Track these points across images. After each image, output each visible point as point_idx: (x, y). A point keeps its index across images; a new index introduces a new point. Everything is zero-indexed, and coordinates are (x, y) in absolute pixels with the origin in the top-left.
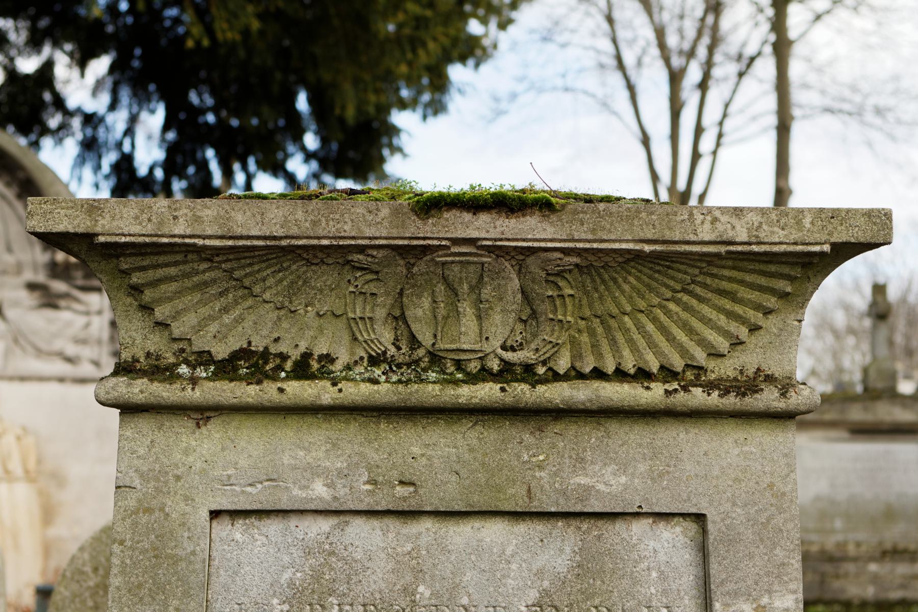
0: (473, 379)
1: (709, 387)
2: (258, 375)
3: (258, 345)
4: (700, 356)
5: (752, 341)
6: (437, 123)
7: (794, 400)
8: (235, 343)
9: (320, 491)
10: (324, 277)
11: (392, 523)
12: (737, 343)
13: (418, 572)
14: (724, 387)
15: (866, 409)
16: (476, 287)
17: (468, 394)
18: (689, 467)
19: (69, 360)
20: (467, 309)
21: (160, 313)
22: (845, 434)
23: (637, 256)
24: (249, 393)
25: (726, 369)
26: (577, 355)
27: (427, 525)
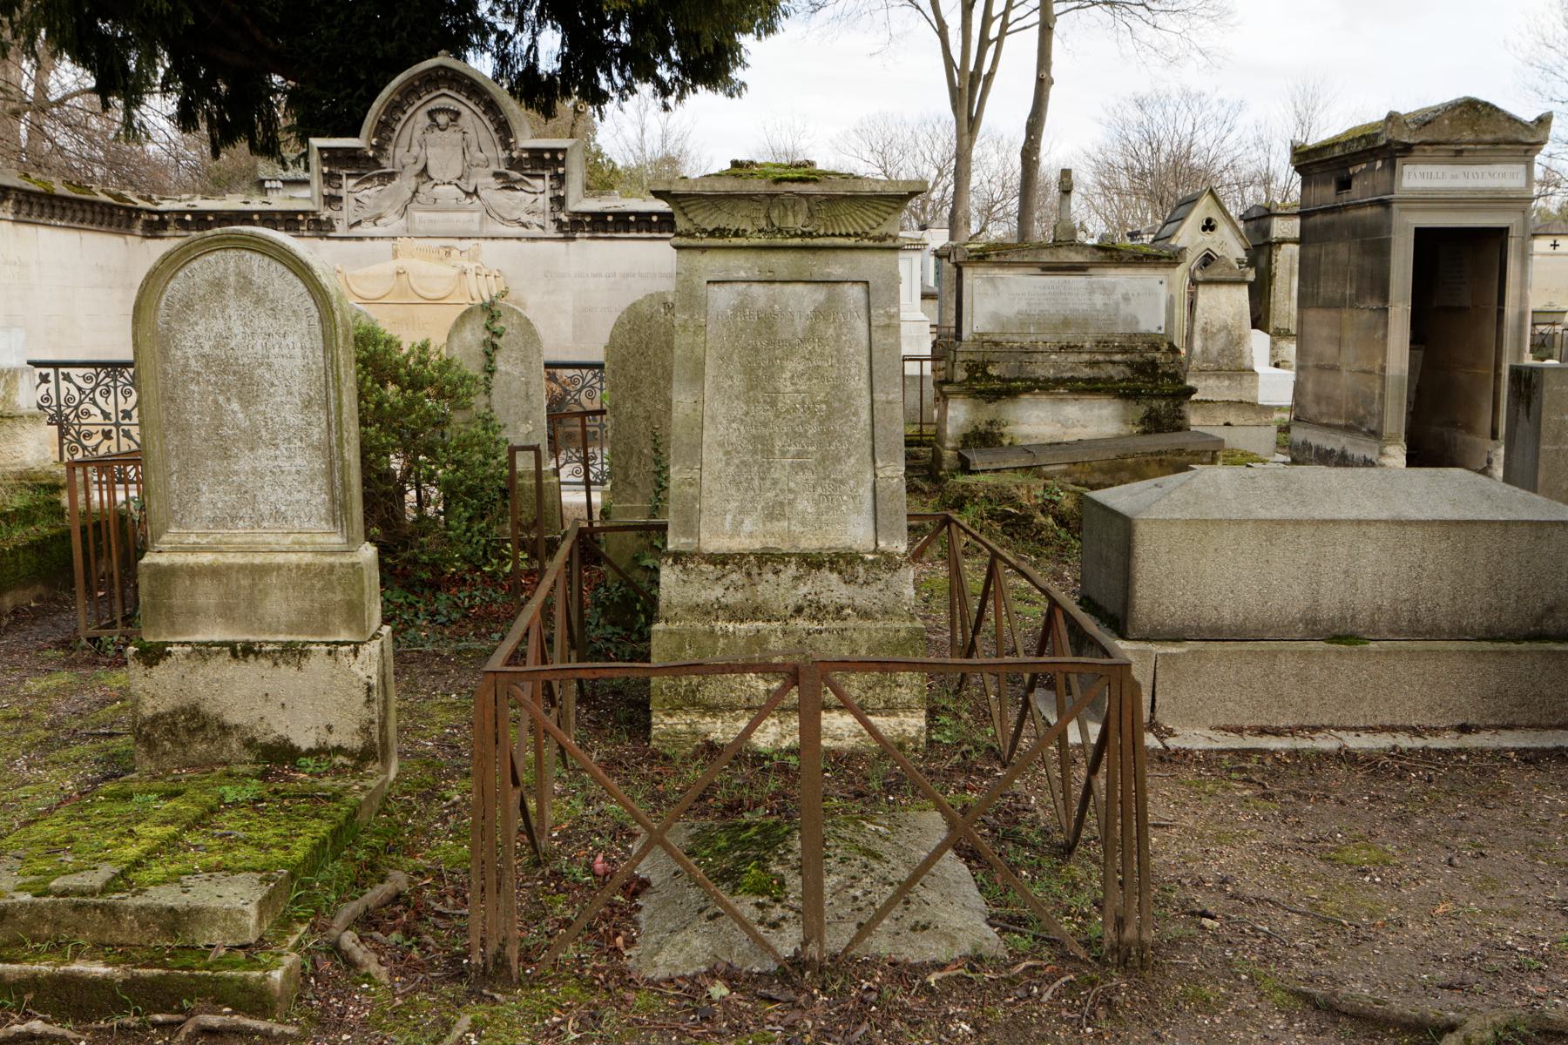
0: (792, 237)
1: (870, 239)
2: (722, 236)
3: (722, 226)
4: (867, 229)
5: (884, 224)
6: (770, 41)
7: (898, 243)
8: (714, 226)
9: (742, 275)
10: (744, 204)
11: (766, 285)
12: (879, 224)
13: (775, 301)
14: (875, 239)
15: (1052, 254)
16: (793, 207)
17: (790, 242)
18: (863, 265)
19: (524, 225)
20: (790, 213)
21: (690, 216)
22: (1039, 271)
23: (845, 196)
24: (720, 242)
25: (876, 233)
26: (826, 229)
27: (777, 285)
